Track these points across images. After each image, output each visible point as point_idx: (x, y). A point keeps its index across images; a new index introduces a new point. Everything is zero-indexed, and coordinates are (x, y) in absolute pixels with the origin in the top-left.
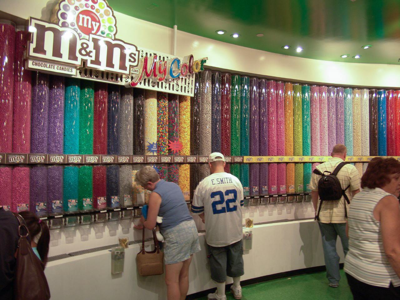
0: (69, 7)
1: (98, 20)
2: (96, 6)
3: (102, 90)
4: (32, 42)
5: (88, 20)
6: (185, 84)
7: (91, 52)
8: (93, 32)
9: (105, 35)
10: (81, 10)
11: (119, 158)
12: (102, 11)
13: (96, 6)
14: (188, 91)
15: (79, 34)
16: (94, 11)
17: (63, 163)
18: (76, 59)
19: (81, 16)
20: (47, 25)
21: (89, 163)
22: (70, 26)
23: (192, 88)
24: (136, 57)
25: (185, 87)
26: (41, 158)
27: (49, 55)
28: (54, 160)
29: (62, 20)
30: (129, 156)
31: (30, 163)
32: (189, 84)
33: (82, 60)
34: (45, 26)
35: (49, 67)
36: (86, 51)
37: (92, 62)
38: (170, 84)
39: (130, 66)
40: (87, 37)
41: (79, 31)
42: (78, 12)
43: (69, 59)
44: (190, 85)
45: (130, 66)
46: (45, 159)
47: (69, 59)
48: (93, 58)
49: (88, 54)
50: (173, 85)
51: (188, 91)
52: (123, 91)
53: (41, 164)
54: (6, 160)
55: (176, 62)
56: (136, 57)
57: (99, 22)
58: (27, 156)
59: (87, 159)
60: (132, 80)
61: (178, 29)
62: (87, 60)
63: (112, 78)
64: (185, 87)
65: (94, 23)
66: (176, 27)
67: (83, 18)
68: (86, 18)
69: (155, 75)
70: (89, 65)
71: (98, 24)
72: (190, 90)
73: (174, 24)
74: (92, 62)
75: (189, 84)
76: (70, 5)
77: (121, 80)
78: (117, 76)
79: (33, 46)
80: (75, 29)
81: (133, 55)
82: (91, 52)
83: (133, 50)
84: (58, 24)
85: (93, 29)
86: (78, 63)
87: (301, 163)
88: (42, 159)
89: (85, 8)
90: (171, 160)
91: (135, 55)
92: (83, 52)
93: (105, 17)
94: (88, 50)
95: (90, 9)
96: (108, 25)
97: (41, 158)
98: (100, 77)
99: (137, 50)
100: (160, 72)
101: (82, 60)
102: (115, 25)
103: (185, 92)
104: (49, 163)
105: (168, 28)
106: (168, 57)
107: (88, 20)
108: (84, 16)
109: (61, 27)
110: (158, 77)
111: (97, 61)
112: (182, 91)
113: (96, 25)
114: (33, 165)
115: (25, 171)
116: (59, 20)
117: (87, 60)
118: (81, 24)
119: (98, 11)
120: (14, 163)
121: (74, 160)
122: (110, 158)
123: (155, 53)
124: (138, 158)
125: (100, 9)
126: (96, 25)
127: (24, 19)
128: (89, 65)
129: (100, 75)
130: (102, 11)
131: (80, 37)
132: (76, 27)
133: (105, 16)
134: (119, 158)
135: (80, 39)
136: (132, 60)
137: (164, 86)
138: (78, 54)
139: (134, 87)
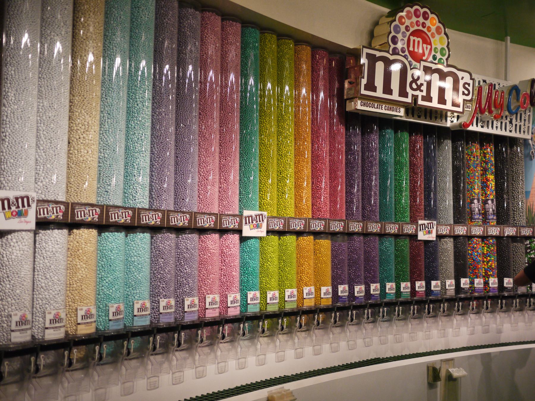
0: (400, 28)
1: (429, 41)
2: (428, 23)
3: (402, 131)
4: (363, 78)
5: (419, 42)
6: (517, 121)
7: (422, 84)
8: (424, 58)
9: (436, 62)
10: (412, 30)
11: (473, 229)
12: (433, 28)
13: (428, 23)
14: (524, 132)
15: (410, 62)
16: (425, 30)
17: (100, 223)
18: (406, 95)
19: (412, 38)
20: (378, 54)
21: (146, 226)
22: (401, 53)
23: (529, 127)
24: (470, 88)
25: (520, 126)
26: (125, 215)
27: (379, 93)
28: (83, 215)
29: (392, 46)
30: (450, 225)
31: (74, 222)
32: (525, 120)
33: (413, 95)
34: (376, 55)
35: (377, 108)
36: (417, 84)
37: (424, 99)
38: (502, 123)
39: (464, 100)
40: (418, 64)
41: (410, 59)
42: (408, 34)
43: (400, 96)
44: (527, 122)
45: (464, 100)
46: (65, 211)
47: (400, 96)
48: (424, 93)
49: (419, 88)
50: (506, 124)
51: (524, 132)
52: (444, 133)
53: (358, 234)
54: (71, 214)
55: (514, 91)
56: (470, 88)
57: (430, 44)
58: (68, 206)
59: (77, 212)
60: (457, 120)
61: (511, 42)
62: (418, 96)
63: (436, 118)
64: (520, 126)
65: (425, 46)
66: (509, 38)
67: (414, 41)
68: (417, 39)
69: (490, 112)
70: (420, 102)
71: (429, 47)
72: (526, 130)
73: (506, 36)
74: (424, 99)
75: (525, 120)
76: (401, 26)
77: (446, 121)
78: (441, 114)
79: (364, 81)
80: (406, 55)
81: (467, 86)
82: (422, 84)
83: (467, 76)
84: (388, 52)
85: (424, 54)
86: (409, 100)
87: (450, 236)
88: (60, 212)
89: (416, 28)
90: (483, 232)
91: (469, 85)
92: (414, 86)
93: (437, 37)
94: (419, 83)
95: (420, 28)
96: (439, 47)
97: (125, 215)
98: (423, 117)
99: (471, 79)
100: (495, 107)
101: (413, 95)
102: (448, 46)
103: (506, 131)
104: (139, 225)
105: (492, 40)
106: (499, 84)
107: (419, 42)
108: (415, 38)
109: (392, 55)
110: (494, 114)
111: (428, 98)
112: (501, 130)
113: (427, 48)
114: (351, 234)
115: (358, 241)
116: (390, 46)
117: (418, 96)
118: (411, 49)
119: (429, 29)
120: (46, 220)
121: (48, 214)
122: (92, 210)
123: (484, 79)
124: (460, 228)
125: (431, 26)
126: (427, 48)
127: (345, 47)
128: (420, 102)
129: (423, 113)
130: (433, 28)
131: (411, 65)
132: (407, 53)
133: (436, 35)
134: (489, 229)
135: (411, 69)
136: (466, 92)
137: (495, 126)
138: (408, 89)
139: (465, 129)
